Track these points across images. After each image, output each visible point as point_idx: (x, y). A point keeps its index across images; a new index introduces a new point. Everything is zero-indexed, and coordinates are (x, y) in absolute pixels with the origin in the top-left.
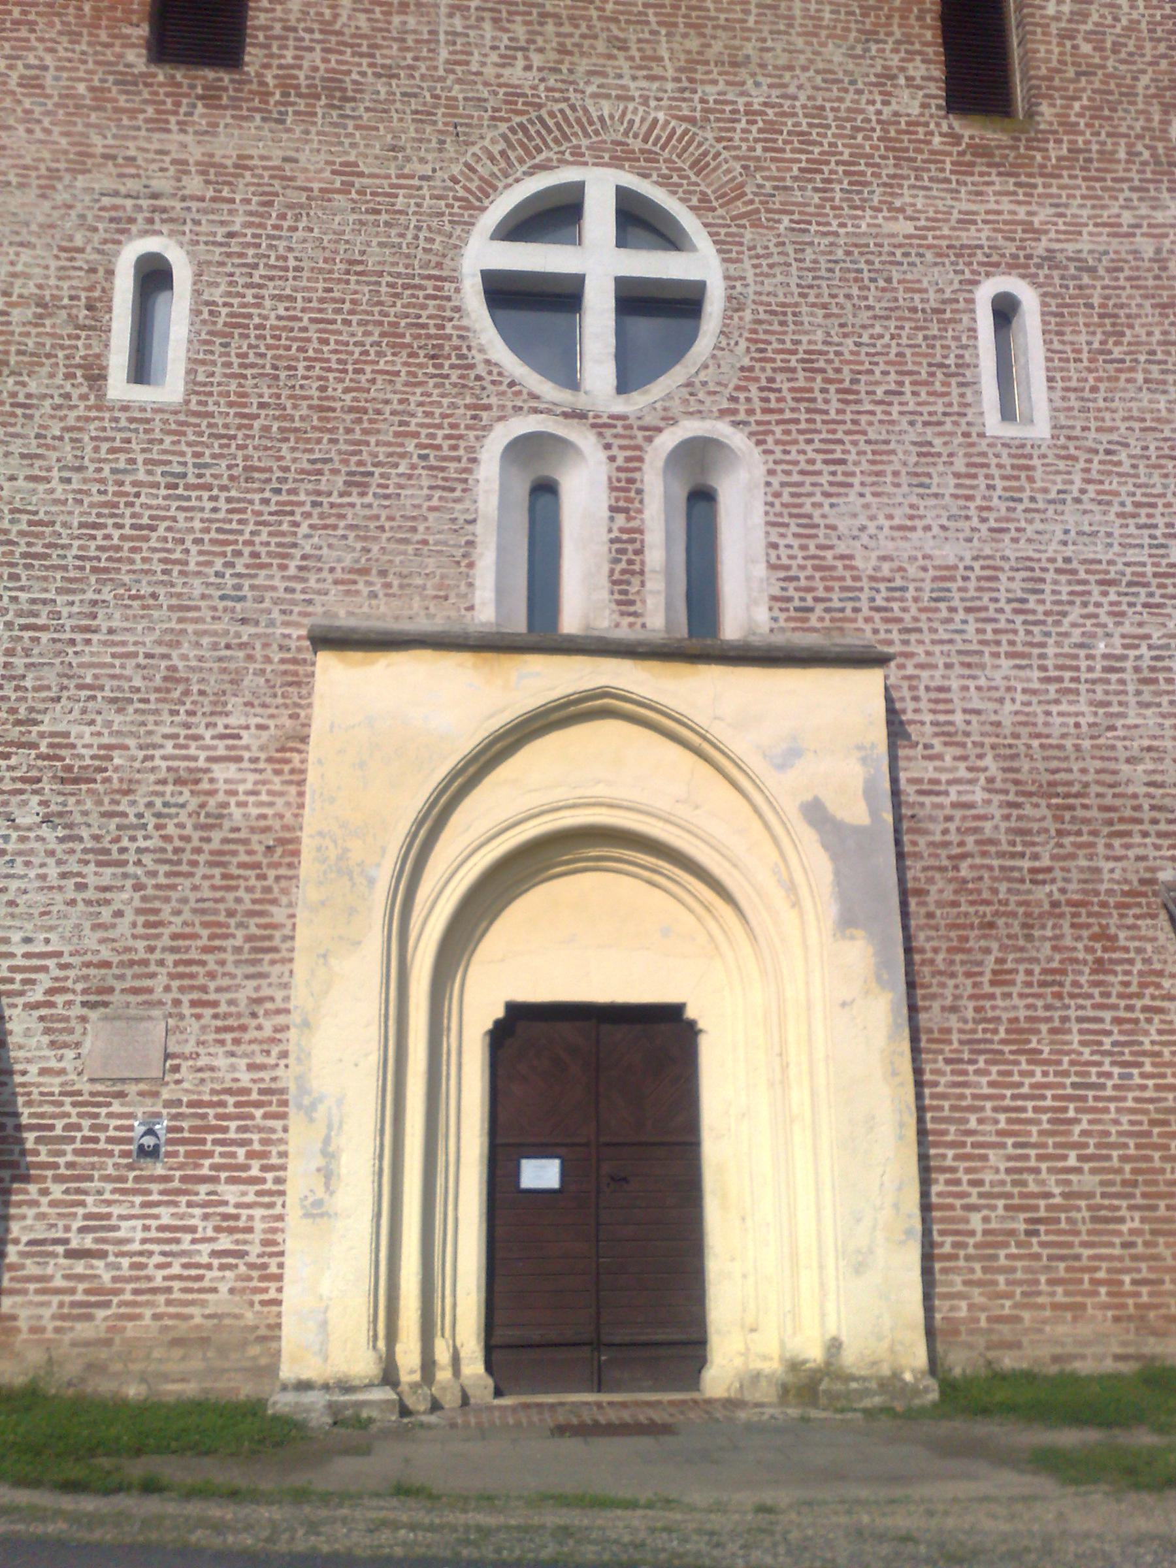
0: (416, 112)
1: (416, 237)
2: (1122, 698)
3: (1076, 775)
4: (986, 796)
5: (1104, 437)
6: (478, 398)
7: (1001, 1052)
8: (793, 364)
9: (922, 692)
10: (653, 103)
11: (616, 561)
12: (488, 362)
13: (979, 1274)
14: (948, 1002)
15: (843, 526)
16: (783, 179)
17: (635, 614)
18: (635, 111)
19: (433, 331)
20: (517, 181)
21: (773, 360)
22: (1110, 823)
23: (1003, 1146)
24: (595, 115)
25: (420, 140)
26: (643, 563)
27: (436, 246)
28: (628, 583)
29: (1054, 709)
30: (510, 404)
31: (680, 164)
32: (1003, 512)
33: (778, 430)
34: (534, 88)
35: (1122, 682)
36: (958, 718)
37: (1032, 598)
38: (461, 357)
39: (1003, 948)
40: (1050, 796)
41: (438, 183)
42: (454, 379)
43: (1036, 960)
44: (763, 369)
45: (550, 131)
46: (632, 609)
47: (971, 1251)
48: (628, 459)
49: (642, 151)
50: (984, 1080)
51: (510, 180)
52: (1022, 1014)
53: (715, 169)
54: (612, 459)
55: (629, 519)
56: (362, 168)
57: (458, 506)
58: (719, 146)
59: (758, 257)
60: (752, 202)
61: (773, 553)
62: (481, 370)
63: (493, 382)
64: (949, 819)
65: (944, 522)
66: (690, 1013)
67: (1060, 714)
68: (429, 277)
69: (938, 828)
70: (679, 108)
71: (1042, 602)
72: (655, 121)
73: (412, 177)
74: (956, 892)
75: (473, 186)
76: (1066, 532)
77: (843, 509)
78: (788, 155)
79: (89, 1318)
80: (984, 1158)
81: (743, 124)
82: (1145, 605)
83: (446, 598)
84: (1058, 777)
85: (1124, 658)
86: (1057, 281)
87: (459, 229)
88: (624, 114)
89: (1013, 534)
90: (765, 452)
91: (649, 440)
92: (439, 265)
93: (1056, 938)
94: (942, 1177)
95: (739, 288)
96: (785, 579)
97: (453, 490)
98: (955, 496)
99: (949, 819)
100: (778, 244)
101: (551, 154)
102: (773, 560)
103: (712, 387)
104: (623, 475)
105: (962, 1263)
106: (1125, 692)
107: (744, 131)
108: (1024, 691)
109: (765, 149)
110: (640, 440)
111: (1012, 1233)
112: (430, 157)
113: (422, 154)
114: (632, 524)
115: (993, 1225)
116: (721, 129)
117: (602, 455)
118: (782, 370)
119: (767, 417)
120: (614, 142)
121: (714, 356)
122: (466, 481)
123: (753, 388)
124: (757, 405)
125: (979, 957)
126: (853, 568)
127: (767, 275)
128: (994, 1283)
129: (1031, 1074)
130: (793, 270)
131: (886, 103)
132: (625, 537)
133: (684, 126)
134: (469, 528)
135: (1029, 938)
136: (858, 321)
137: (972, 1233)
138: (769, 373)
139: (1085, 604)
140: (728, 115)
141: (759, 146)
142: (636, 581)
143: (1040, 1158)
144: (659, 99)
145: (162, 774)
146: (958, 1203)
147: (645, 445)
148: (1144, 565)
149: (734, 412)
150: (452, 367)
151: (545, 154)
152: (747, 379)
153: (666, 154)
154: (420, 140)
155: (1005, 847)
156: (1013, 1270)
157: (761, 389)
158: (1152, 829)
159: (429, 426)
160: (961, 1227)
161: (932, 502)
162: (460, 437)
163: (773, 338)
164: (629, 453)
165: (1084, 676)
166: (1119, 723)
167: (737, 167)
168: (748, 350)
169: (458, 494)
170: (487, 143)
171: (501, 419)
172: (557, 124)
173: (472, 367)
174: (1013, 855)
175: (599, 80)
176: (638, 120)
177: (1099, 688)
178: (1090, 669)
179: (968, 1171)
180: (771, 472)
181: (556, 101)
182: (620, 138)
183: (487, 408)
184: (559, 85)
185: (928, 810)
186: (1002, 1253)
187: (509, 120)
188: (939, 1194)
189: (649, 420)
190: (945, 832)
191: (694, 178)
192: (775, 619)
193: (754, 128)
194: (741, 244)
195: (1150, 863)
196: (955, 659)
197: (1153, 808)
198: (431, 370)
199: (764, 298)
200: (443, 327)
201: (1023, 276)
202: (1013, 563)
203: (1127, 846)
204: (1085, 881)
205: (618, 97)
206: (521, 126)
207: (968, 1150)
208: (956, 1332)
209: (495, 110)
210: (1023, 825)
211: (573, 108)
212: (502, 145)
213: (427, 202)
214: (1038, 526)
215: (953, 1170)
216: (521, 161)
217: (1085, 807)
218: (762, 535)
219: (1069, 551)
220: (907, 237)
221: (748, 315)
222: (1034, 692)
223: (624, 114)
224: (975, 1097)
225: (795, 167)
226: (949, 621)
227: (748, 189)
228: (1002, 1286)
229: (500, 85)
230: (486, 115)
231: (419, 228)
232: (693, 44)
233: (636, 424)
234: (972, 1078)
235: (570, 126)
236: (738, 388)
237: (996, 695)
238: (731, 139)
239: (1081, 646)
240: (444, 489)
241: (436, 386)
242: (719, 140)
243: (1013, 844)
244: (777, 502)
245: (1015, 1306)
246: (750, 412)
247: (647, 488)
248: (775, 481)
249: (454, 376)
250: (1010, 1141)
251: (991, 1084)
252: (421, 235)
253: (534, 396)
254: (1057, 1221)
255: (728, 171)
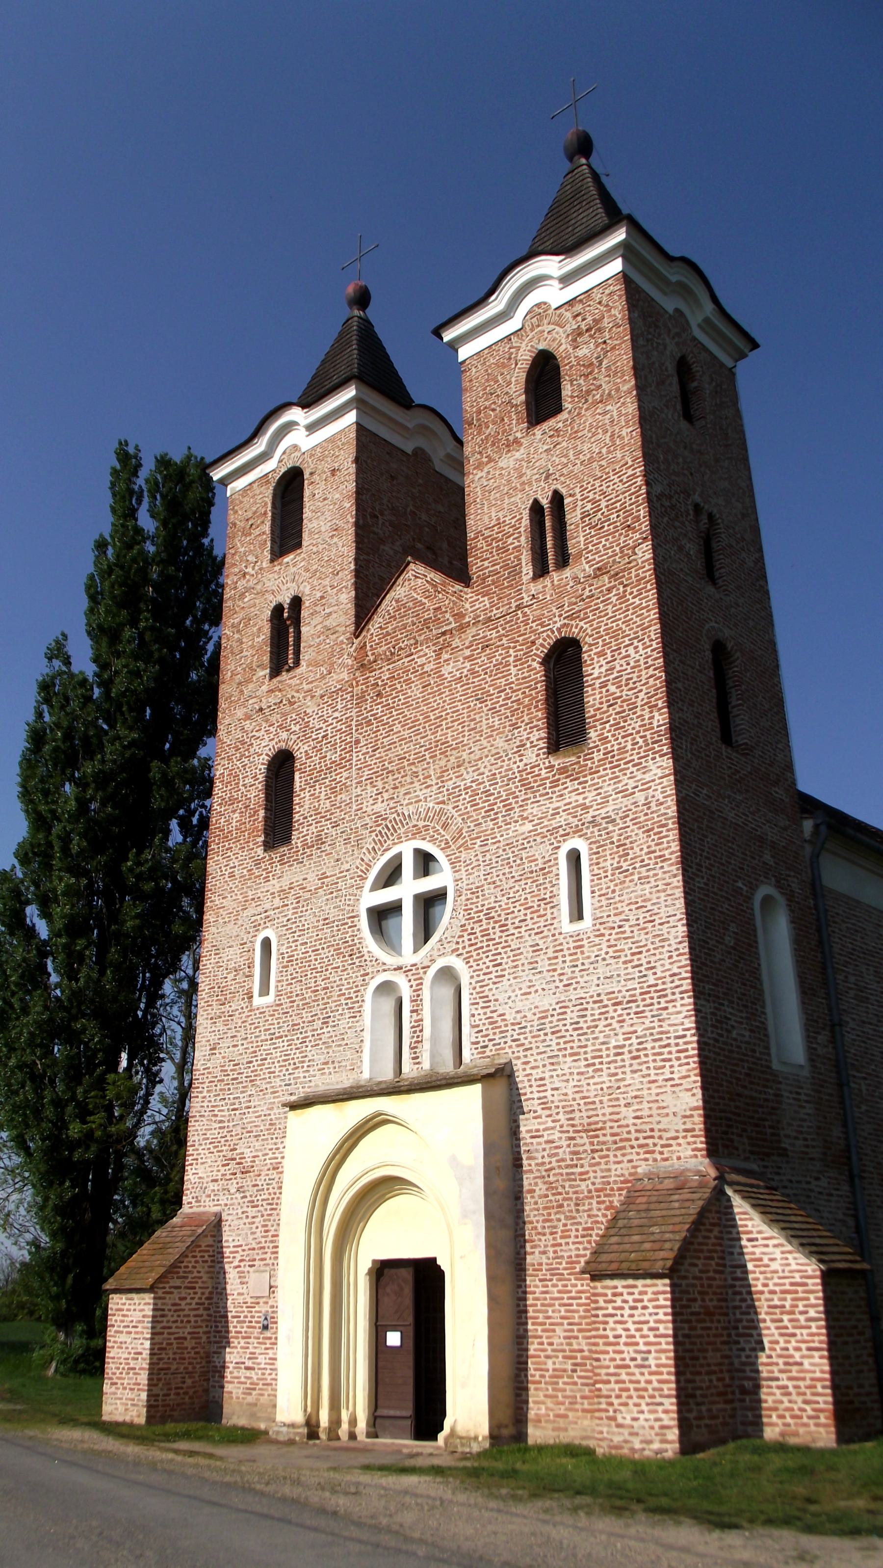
2: (623, 1070)
3: (601, 1118)
4: (560, 1135)
5: (617, 919)
7: (563, 1274)
9: (533, 1083)
13: (550, 1392)
14: (542, 1249)
15: (502, 997)
22: (615, 1142)
23: (562, 1324)
29: (591, 1081)
32: (570, 975)
35: (623, 1060)
36: (548, 1094)
37: (581, 1020)
39: (567, 1218)
40: (589, 1131)
43: (580, 1223)
47: (547, 1379)
50: (555, 1289)
52: (573, 1253)
56: (328, 874)
64: (544, 1150)
65: (544, 986)
67: (595, 1084)
69: (539, 1155)
71: (586, 1022)
74: (547, 1189)
76: (599, 978)
77: (501, 989)
79: (250, 1394)
80: (554, 1331)
82: (636, 1013)
84: (592, 1120)
85: (624, 1046)
86: (597, 834)
89: (574, 986)
91: (425, 973)
93: (590, 1210)
94: (536, 1341)
98: (549, 971)
99: (544, 1150)
105: (543, 1385)
106: (624, 1066)
108: (578, 1074)
111: (565, 1371)
115: (557, 1366)
125: (555, 1223)
126: (505, 1020)
128: (557, 1397)
129: (576, 1286)
131: (521, 761)
135: (578, 1211)
136: (508, 886)
137: (548, 1370)
139: (606, 1019)
143: (580, 1331)
145: (269, 1166)
146: (542, 1354)
148: (635, 989)
155: (569, 1162)
156: (565, 1390)
158: (634, 1143)
160: (543, 1367)
161: (539, 976)
165: (605, 1060)
166: (622, 1084)
174: (572, 1166)
177: (612, 1066)
178: (608, 1056)
179: (548, 1337)
185: (535, 1147)
186: (561, 1381)
188: (535, 1350)
190: (543, 1157)
195: (634, 1164)
196: (547, 1062)
197: (637, 1131)
201: (580, 836)
202: (574, 1003)
203: (624, 1155)
204: (603, 1177)
207: (547, 1326)
208: (540, 1421)
210: (576, 1149)
214: (586, 978)
215: (541, 1337)
217: (604, 1135)
219: (600, 990)
220: (530, 832)
221: (463, 898)
222: (582, 1073)
224: (551, 1299)
226: (545, 1041)
228: (560, 1399)
232: (443, 763)
234: (550, 1289)
237: (565, 1078)
239: (603, 1043)
243: (572, 1160)
245: (566, 1409)
248: (473, 981)
250: (566, 1322)
251: (559, 1292)
254: (585, 1365)
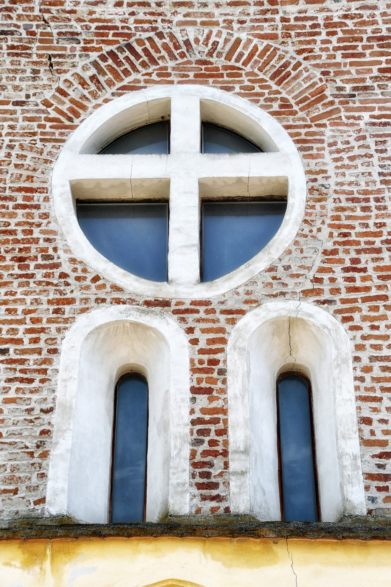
0: (13, 47)
1: (9, 155)
6: (61, 293)
8: (378, 244)
10: (236, 26)
11: (199, 442)
12: (73, 261)
16: (363, 80)
17: (217, 498)
18: (219, 34)
19: (20, 236)
20: (106, 101)
21: (358, 243)
24: (181, 39)
25: (15, 71)
26: (226, 443)
27: (27, 162)
28: (211, 465)
30: (93, 297)
31: (261, 76)
33: (365, 307)
34: (124, 21)
38: (50, 257)
41: (31, 107)
42: (39, 277)
44: (347, 252)
45: (138, 56)
46: (214, 492)
48: (211, 341)
49: (225, 68)
51: (100, 101)
53: (295, 78)
54: (194, 342)
55: (211, 400)
57: (35, 397)
58: (300, 58)
59: (338, 151)
60: (332, 103)
61: (366, 429)
62: (66, 268)
63: (78, 279)
66: (193, 300)
68: (20, 190)
70: (261, 28)
72: (238, 41)
73: (7, 103)
75: (64, 108)
78: (368, 59)
81: (324, 36)
83: (15, 492)
87: (49, 145)
88: (208, 37)
90: (352, 328)
91: (233, 322)
92: (30, 178)
95: (321, 181)
96: (380, 456)
97: (31, 381)
100: (358, 139)
101: (139, 76)
102: (367, 436)
103: (294, 270)
104: (205, 357)
107: (323, 42)
109: (345, 56)
110: (222, 324)
112: (23, 85)
113: (17, 83)
114: (214, 405)
116: (301, 42)
117: (185, 339)
118: (365, 251)
119: (353, 295)
120: (200, 62)
121: (296, 243)
122: (45, 371)
123: (338, 268)
124: (342, 284)
127: (348, 167)
130: (375, 160)
132: (207, 417)
133: (266, 42)
134: (46, 417)
138: (353, 255)
140: (308, 30)
141: (339, 54)
142: (218, 462)
144: (242, 22)
147: (228, 327)
149: (319, 292)
150: (38, 267)
151: (134, 76)
152: (329, 261)
153: (248, 68)
154: (15, 71)
157: (346, 270)
159: (11, 322)
162: (43, 330)
163: (356, 223)
164: (212, 336)
167: (317, 73)
168: (331, 235)
169: (36, 384)
170: (78, 70)
171: (83, 311)
172: (145, 50)
173: (57, 266)
175: (183, 10)
176: (221, 41)
180: (359, 347)
181: (144, 30)
182: (204, 58)
183: (70, 301)
184: (149, 17)
187: (100, 49)
189: (231, 305)
191: (275, 87)
192: (373, 500)
193: (334, 39)
194: (322, 141)
198: (17, 271)
199: (346, 188)
200: (31, 232)
205: (203, 24)
206: (112, 54)
209: (86, 42)
211: (160, 35)
212: (93, 71)
213: (21, 123)
216: (110, 83)
218: (354, 411)
221: (330, 204)
223: (208, 37)
225: (375, 68)
227: (327, 92)
229: (92, 21)
230: (78, 47)
231: (11, 147)
233: (219, 308)
235: (158, 51)
236: (321, 270)
238: (311, 51)
240: (22, 380)
241: (21, 285)
242: (300, 52)
244: (368, 377)
246: (337, 291)
247: (230, 366)
248: (365, 356)
249: (39, 275)
252: (14, 153)
253: (116, 288)
255: (309, 78)
